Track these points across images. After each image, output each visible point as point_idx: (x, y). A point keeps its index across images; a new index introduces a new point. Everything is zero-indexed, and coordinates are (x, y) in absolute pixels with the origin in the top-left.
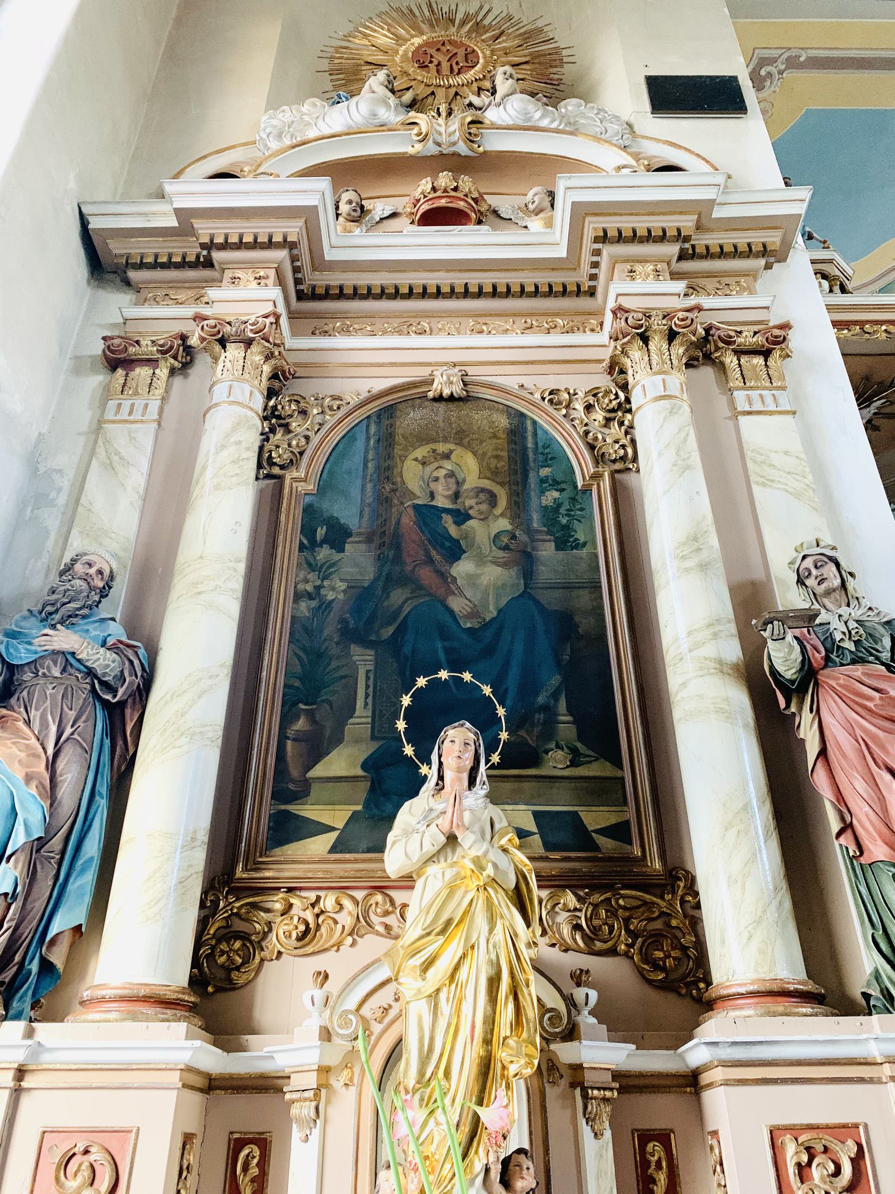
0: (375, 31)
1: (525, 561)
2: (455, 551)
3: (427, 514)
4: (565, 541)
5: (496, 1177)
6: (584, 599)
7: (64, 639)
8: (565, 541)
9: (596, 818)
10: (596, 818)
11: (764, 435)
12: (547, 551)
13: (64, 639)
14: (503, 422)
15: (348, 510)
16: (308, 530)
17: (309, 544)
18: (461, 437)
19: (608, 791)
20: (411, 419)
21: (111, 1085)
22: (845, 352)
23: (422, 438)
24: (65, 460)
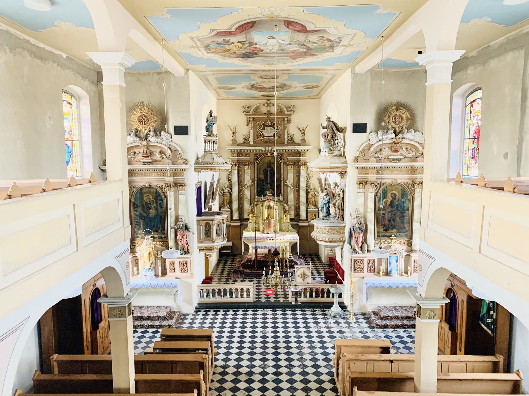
1: (157, 209)
2: (150, 208)
3: (147, 203)
4: (161, 207)
5: (394, 273)
6: (163, 214)
8: (161, 207)
9: (163, 236)
10: (163, 236)
11: (181, 198)
12: (159, 208)
14: (155, 190)
15: (138, 203)
16: (134, 206)
17: (135, 208)
18: (150, 193)
19: (164, 234)
20: (144, 190)
21: (485, 382)
23: (146, 193)
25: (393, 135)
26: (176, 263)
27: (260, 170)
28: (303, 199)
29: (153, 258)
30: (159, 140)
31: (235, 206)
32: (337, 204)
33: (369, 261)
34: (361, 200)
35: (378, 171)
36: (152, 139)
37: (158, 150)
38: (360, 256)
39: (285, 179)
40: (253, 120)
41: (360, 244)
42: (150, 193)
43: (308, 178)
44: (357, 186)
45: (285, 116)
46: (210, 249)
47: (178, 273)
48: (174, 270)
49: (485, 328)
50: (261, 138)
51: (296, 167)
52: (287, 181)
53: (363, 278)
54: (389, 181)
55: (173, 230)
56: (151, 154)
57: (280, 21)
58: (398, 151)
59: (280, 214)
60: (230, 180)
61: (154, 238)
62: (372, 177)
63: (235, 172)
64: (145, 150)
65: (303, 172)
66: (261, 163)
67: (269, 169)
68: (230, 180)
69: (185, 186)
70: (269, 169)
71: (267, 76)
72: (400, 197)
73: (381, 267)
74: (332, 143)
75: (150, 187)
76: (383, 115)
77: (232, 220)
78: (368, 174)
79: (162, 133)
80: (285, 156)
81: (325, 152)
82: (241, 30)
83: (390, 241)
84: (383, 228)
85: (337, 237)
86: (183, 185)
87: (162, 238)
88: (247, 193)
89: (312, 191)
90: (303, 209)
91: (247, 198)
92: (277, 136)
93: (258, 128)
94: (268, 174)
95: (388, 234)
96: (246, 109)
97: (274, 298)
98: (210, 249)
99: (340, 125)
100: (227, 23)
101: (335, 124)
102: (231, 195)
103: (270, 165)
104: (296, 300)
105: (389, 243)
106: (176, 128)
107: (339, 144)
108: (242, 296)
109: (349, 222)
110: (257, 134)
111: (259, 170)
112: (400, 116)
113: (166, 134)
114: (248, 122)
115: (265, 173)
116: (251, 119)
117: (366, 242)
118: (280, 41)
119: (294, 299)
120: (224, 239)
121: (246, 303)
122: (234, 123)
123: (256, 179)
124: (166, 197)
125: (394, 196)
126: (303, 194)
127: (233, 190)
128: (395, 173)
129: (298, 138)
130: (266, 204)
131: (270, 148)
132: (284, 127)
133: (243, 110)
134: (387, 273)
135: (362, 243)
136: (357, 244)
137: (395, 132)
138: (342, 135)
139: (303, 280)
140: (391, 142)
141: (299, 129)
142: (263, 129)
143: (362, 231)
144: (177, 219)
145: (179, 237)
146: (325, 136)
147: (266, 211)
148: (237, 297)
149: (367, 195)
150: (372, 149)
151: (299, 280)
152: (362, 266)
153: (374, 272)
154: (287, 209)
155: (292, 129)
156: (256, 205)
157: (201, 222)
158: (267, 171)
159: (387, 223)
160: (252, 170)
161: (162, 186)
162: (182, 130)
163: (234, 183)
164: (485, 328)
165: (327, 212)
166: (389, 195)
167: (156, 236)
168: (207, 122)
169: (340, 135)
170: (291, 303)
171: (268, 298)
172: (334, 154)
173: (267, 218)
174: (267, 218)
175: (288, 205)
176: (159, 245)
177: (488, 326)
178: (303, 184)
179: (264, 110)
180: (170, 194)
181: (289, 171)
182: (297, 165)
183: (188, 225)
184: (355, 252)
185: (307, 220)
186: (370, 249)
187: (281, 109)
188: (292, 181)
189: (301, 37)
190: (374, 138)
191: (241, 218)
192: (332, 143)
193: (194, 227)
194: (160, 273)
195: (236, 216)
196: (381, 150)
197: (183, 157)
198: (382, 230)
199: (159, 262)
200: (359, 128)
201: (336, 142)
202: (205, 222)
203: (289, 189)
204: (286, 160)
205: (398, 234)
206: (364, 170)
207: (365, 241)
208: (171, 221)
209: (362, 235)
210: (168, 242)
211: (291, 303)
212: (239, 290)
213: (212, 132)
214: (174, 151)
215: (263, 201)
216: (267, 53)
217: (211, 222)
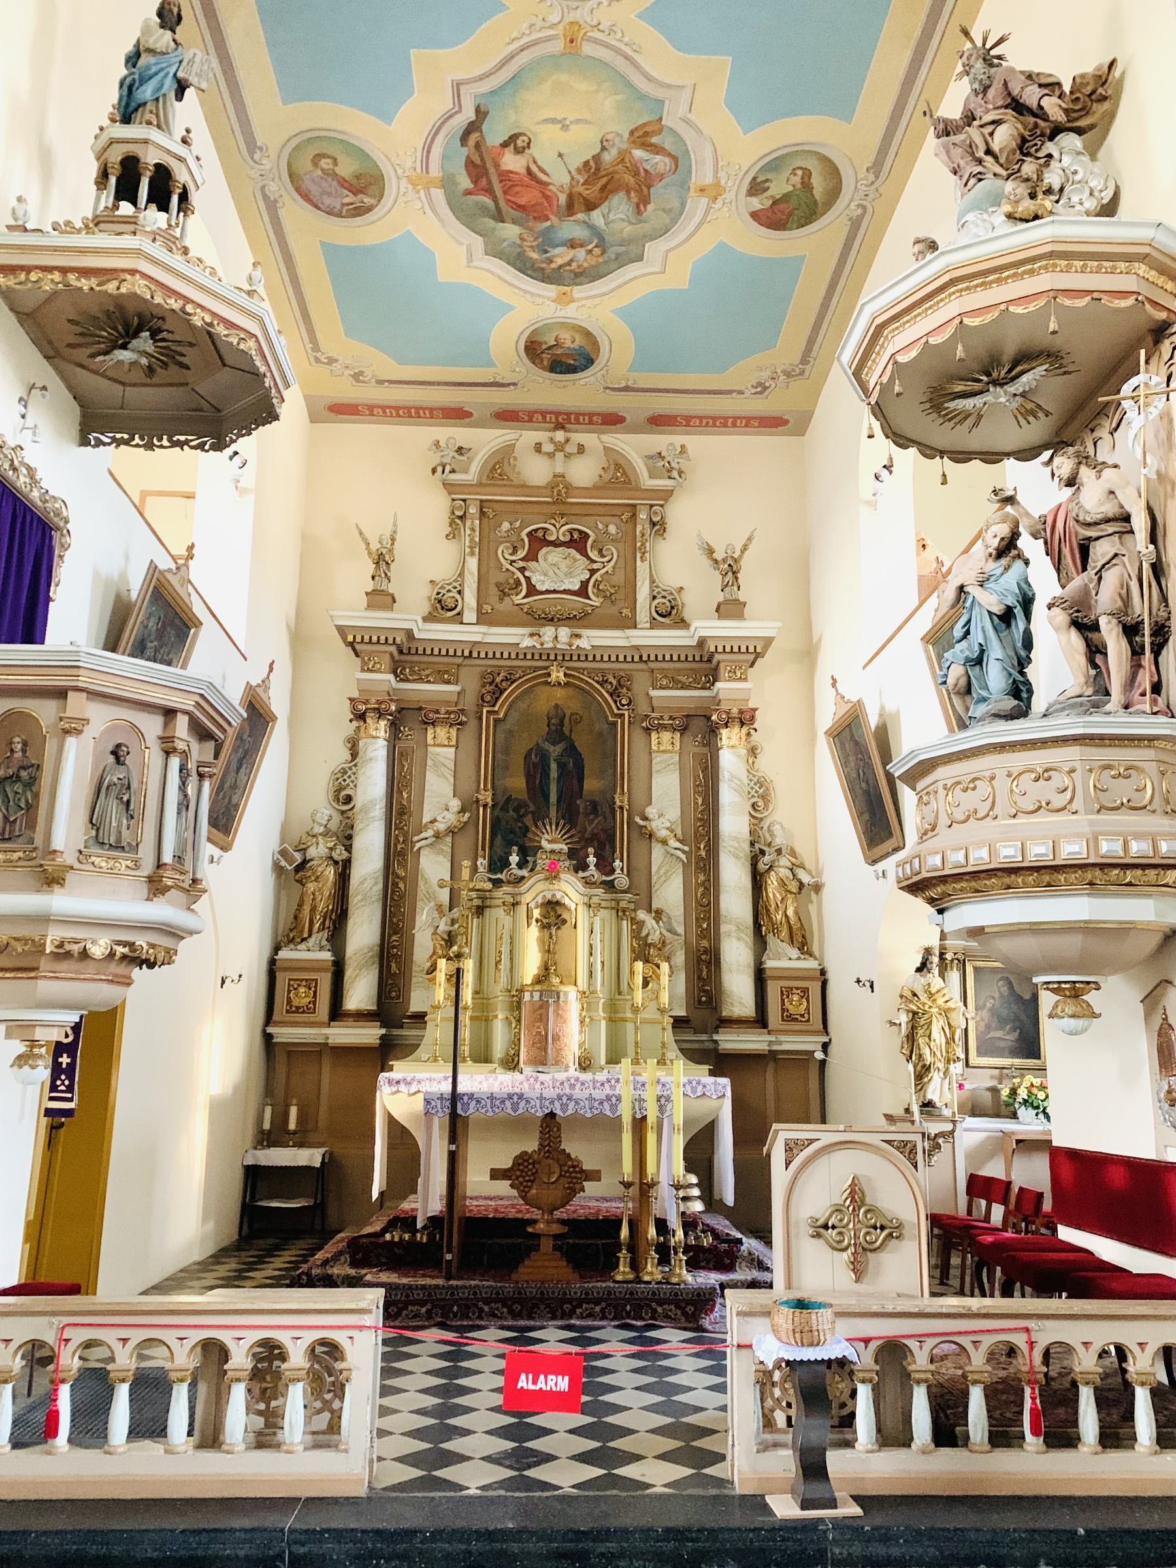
27: (507, 751)
28: (735, 902)
31: (363, 932)
39: (639, 795)
40: (482, 513)
45: (631, 512)
50: (518, 599)
51: (694, 747)
52: (651, 811)
59: (610, 965)
60: (344, 799)
63: (376, 750)
66: (514, 715)
67: (555, 750)
68: (344, 799)
70: (555, 750)
77: (337, 1013)
80: (640, 683)
88: (433, 867)
89: (784, 861)
90: (736, 954)
93: (503, 552)
97: (584, 1458)
102: (344, 870)
103: (559, 728)
104: (813, 1468)
110: (501, 578)
111: (500, 753)
114: (458, 519)
115: (536, 768)
116: (473, 510)
119: (785, 1463)
121: (287, 1503)
123: (487, 797)
126: (733, 875)
127: (358, 843)
130: (534, 891)
132: (633, 551)
133: (435, 460)
139: (858, 1269)
142: (532, 556)
147: (531, 936)
148: (210, 1437)
151: (818, 1269)
154: (654, 938)
155: (675, 563)
156: (480, 911)
158: (544, 757)
163: (366, 809)
170: (757, 1503)
171: (523, 1459)
174: (538, 980)
175: (658, 915)
178: (733, 824)
179: (536, 471)
181: (657, 759)
182: (702, 728)
185: (760, 1020)
187: (618, 466)
195: (360, 992)
203: (657, 851)
211: (757, 1503)
212: (240, 1359)
217: (44, 711)
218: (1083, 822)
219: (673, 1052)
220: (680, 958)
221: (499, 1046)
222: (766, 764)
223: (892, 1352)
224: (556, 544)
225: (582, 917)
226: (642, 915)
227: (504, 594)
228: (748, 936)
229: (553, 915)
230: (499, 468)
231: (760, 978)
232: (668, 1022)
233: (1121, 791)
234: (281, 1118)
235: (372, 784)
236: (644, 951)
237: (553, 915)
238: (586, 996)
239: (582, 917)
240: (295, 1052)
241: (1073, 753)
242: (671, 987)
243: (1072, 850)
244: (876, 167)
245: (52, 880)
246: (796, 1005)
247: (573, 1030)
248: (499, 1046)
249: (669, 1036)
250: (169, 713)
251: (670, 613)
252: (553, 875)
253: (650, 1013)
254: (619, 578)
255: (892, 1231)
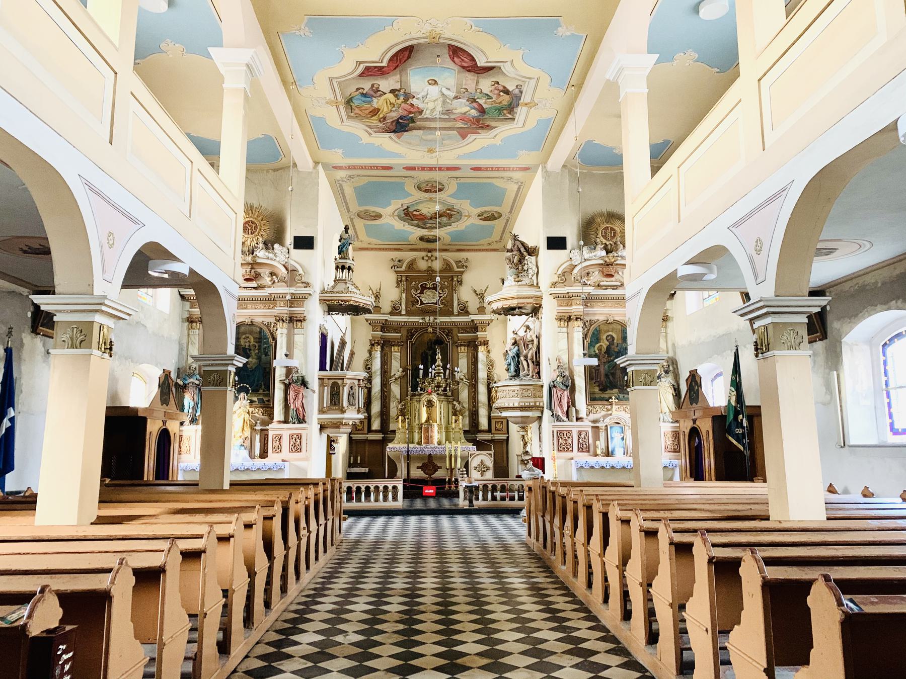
0: (412, 594)
1: (259, 358)
4: (266, 355)
7: (192, 380)
8: (266, 355)
9: (265, 399)
10: (265, 399)
11: (298, 339)
13: (192, 380)
18: (251, 333)
19: (268, 395)
22: (190, 612)
24: (185, 341)
25: (604, 253)
26: (283, 437)
29: (248, 433)
30: (271, 255)
32: (529, 355)
33: (580, 433)
34: (564, 344)
35: (589, 300)
36: (261, 254)
37: (267, 271)
38: (566, 425)
40: (407, 280)
41: (565, 408)
42: (251, 333)
43: (491, 366)
44: (557, 323)
45: (452, 277)
46: (337, 425)
47: (285, 452)
48: (279, 449)
49: (735, 442)
51: (471, 350)
53: (572, 459)
54: (602, 318)
55: (282, 386)
56: (257, 276)
57: (442, 45)
58: (612, 276)
61: (252, 402)
62: (577, 309)
63: (377, 354)
64: (248, 270)
65: (482, 355)
69: (305, 320)
71: (427, 182)
72: (620, 342)
73: (598, 442)
74: (520, 268)
75: (252, 324)
76: (588, 231)
77: (370, 431)
78: (571, 305)
79: (276, 246)
80: (455, 331)
81: (510, 281)
82: (395, 65)
83: (609, 407)
84: (599, 386)
85: (531, 401)
86: (302, 320)
87: (263, 402)
88: (395, 389)
90: (483, 412)
91: (395, 397)
92: (442, 303)
94: (428, 342)
95: (607, 396)
96: (396, 263)
98: (337, 425)
99: (530, 244)
100: (376, 51)
101: (523, 244)
104: (471, 502)
105: (608, 410)
106: (297, 239)
107: (530, 271)
108: (385, 498)
109: (548, 374)
111: (414, 354)
112: (612, 229)
113: (281, 248)
114: (399, 282)
117: (574, 405)
118: (444, 90)
119: (467, 502)
120: (359, 411)
122: (375, 279)
123: (410, 367)
124: (274, 339)
125: (611, 339)
128: (611, 307)
129: (473, 304)
130: (425, 398)
131: (432, 318)
132: (452, 290)
134: (608, 453)
135: (569, 407)
136: (561, 406)
137: (605, 248)
138: (533, 258)
139: (476, 468)
140: (602, 262)
141: (475, 292)
142: (422, 293)
143: (567, 387)
144: (289, 371)
145: (292, 394)
146: (510, 261)
148: (377, 500)
149: (572, 338)
150: (576, 271)
152: (570, 440)
153: (588, 451)
155: (465, 294)
157: (326, 381)
158: (427, 355)
159: (603, 378)
160: (404, 352)
161: (269, 325)
162: (305, 243)
164: (735, 442)
165: (516, 371)
166: (604, 337)
167: (255, 399)
168: (340, 240)
169: (530, 260)
172: (523, 283)
173: (427, 421)
174: (426, 422)
175: (459, 403)
176: (259, 413)
177: (739, 438)
178: (482, 374)
179: (423, 265)
180: (281, 333)
182: (473, 345)
183: (307, 379)
184: (558, 419)
185: (489, 431)
186: (580, 416)
187: (448, 265)
188: (465, 371)
189: (469, 80)
190: (576, 256)
191: (384, 427)
192: (520, 268)
193: (314, 383)
194: (257, 452)
195: (376, 425)
196: (588, 274)
197: (303, 280)
198: (597, 390)
199: (258, 438)
200: (557, 243)
201: (525, 268)
202: (331, 381)
204: (456, 339)
205: (621, 396)
206: (567, 299)
207: (572, 403)
208: (280, 374)
209: (566, 394)
210: (273, 407)
213: (347, 254)
214: (292, 271)
215: (420, 395)
216: (427, 119)
217: (340, 382)
218: (518, 399)
219: (463, 440)
220: (467, 413)
221: (416, 440)
222: (493, 355)
223: (485, 486)
224: (429, 288)
225: (438, 404)
226: (455, 403)
227: (414, 307)
228: (486, 407)
229: (430, 404)
230: (411, 266)
231: (490, 419)
232: (462, 432)
233: (526, 394)
234: (355, 460)
235: (377, 365)
236: (455, 414)
237: (430, 404)
238: (440, 426)
239: (438, 404)
240: (359, 442)
241: (518, 388)
242: (463, 422)
243: (516, 405)
244: (511, 212)
245: (343, 412)
246: (499, 426)
247: (436, 435)
248: (416, 440)
249: (462, 435)
250: (359, 380)
251: (464, 311)
252: (430, 394)
253: (457, 430)
254: (448, 298)
255: (488, 469)
